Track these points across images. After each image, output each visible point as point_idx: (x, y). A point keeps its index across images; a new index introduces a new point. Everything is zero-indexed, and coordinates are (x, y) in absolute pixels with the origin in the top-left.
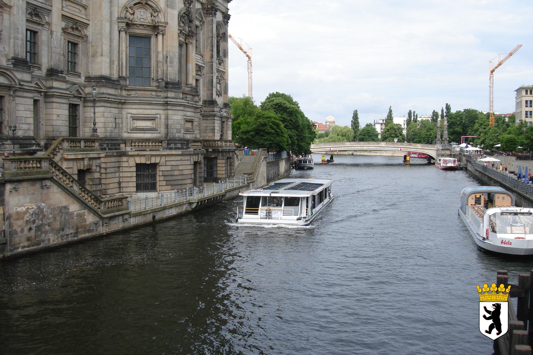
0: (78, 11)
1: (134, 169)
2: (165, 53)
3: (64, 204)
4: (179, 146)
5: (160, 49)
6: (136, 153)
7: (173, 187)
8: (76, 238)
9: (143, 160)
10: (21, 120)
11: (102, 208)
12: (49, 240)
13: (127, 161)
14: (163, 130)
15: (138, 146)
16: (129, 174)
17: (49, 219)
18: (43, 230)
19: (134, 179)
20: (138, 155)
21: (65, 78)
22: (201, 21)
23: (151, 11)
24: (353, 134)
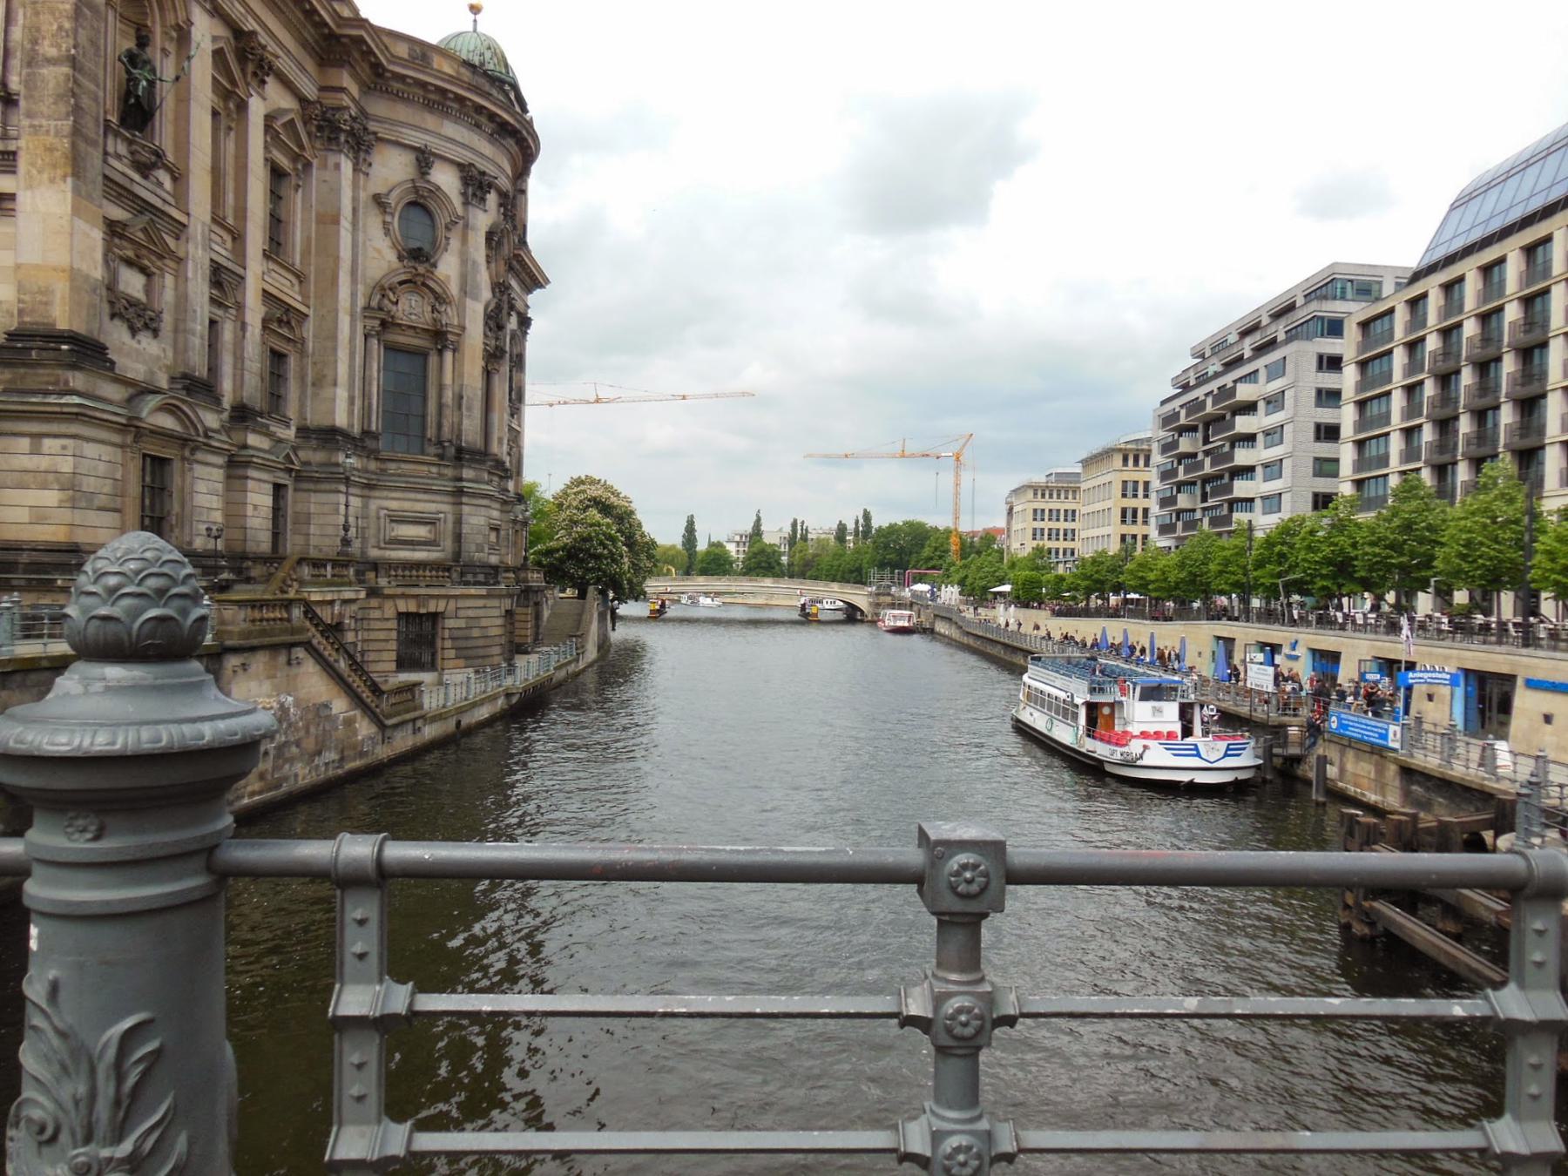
0: (288, 283)
1: (393, 624)
2: (457, 389)
3: (324, 699)
4: (481, 578)
5: (448, 378)
6: (399, 591)
7: (470, 662)
8: (340, 771)
9: (412, 607)
10: (201, 514)
11: (384, 705)
12: (296, 776)
13: (380, 608)
14: (448, 544)
15: (403, 576)
16: (382, 635)
17: (297, 730)
18: (287, 755)
19: (393, 645)
20: (403, 596)
21: (267, 426)
22: (295, 158)
23: (432, 300)
24: (686, 559)
